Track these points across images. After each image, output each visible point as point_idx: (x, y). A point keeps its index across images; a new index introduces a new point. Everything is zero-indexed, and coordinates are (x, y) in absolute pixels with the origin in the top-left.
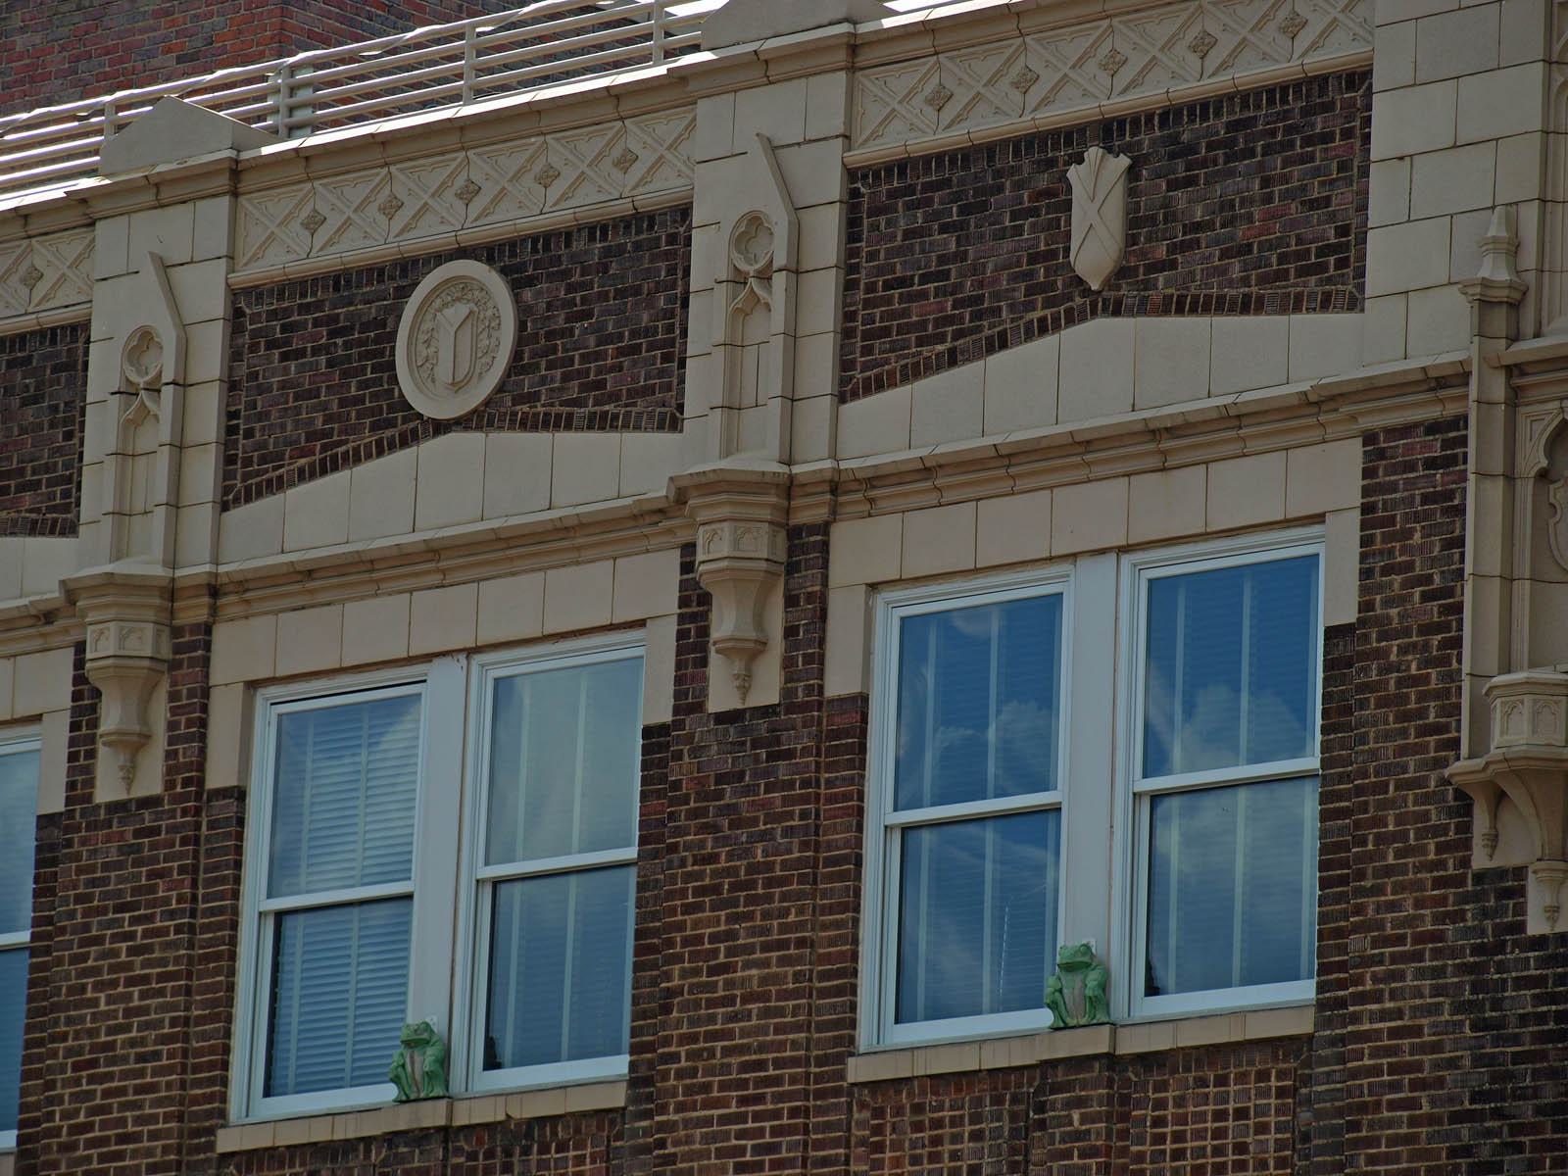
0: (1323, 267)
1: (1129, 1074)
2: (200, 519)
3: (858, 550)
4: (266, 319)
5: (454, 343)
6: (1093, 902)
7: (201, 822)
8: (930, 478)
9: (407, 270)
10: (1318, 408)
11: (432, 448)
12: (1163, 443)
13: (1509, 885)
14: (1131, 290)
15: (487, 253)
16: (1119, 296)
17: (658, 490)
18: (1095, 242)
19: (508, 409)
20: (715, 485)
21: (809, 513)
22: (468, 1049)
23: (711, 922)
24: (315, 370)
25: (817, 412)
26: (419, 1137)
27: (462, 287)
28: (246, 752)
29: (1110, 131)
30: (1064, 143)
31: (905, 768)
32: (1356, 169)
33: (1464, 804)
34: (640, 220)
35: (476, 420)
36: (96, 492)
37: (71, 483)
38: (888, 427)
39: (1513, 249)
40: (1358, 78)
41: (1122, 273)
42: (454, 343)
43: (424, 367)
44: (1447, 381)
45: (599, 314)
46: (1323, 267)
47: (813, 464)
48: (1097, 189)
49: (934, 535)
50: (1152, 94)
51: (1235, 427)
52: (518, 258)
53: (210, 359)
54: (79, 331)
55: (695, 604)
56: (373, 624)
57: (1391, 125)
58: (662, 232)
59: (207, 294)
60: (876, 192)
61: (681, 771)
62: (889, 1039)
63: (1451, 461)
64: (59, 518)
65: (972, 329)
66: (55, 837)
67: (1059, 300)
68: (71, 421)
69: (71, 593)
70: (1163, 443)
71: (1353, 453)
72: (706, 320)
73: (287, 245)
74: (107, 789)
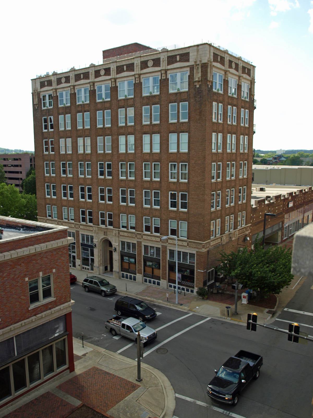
0: (188, 60)
1: (105, 102)
2: (74, 83)
3: (96, 84)
4: (76, 75)
5: (150, 63)
6: (104, 96)
7: (140, 84)
8: (60, 88)
9: (148, 61)
10: (188, 66)
11: (149, 68)
12: (128, 76)
13: (196, 85)
14: (180, 61)
15: (152, 60)
16: (83, 79)
17: (51, 89)
18: (125, 69)
19: (153, 66)
20: (112, 78)
21: (166, 70)
22: (127, 95)
23: (163, 87)
24: (144, 65)
25: (166, 66)
26: (151, 96)
27: (150, 61)
28: (142, 80)
29: (179, 55)
30: (177, 55)
31: (171, 81)
32: (189, 56)
33: (194, 82)
34: (158, 58)
35: (152, 67)
36: (135, 70)
37: (134, 69)
38: (169, 67)
39: (196, 60)
40: (189, 53)
41: (179, 61)
42: (150, 63)
43: (149, 65)
44: (194, 65)
45: (157, 62)
46: (188, 60)
47: (116, 77)
48: (82, 75)
49: (98, 83)
50: (180, 53)
51: (86, 84)
52: (153, 60)
53: (140, 64)
54: (110, 68)
55: (161, 74)
56: (123, 79)
57: (190, 55)
58: (109, 68)
59: (139, 62)
60: (169, 57)
61: (161, 81)
62: (98, 101)
63: (193, 68)
64: (134, 71)
65: (173, 63)
66: (134, 84)
67: (176, 62)
68: (134, 67)
69: (135, 74)
70: (128, 76)
71: (189, 68)
72: (161, 62)
73: (143, 59)
74: (136, 82)
